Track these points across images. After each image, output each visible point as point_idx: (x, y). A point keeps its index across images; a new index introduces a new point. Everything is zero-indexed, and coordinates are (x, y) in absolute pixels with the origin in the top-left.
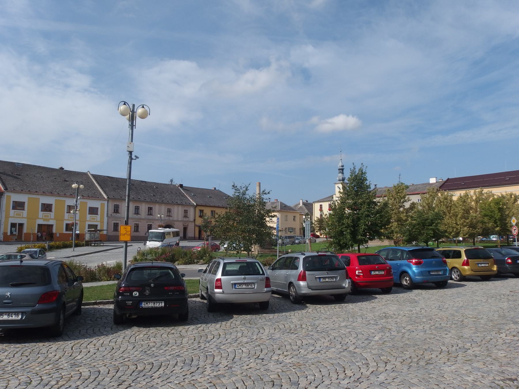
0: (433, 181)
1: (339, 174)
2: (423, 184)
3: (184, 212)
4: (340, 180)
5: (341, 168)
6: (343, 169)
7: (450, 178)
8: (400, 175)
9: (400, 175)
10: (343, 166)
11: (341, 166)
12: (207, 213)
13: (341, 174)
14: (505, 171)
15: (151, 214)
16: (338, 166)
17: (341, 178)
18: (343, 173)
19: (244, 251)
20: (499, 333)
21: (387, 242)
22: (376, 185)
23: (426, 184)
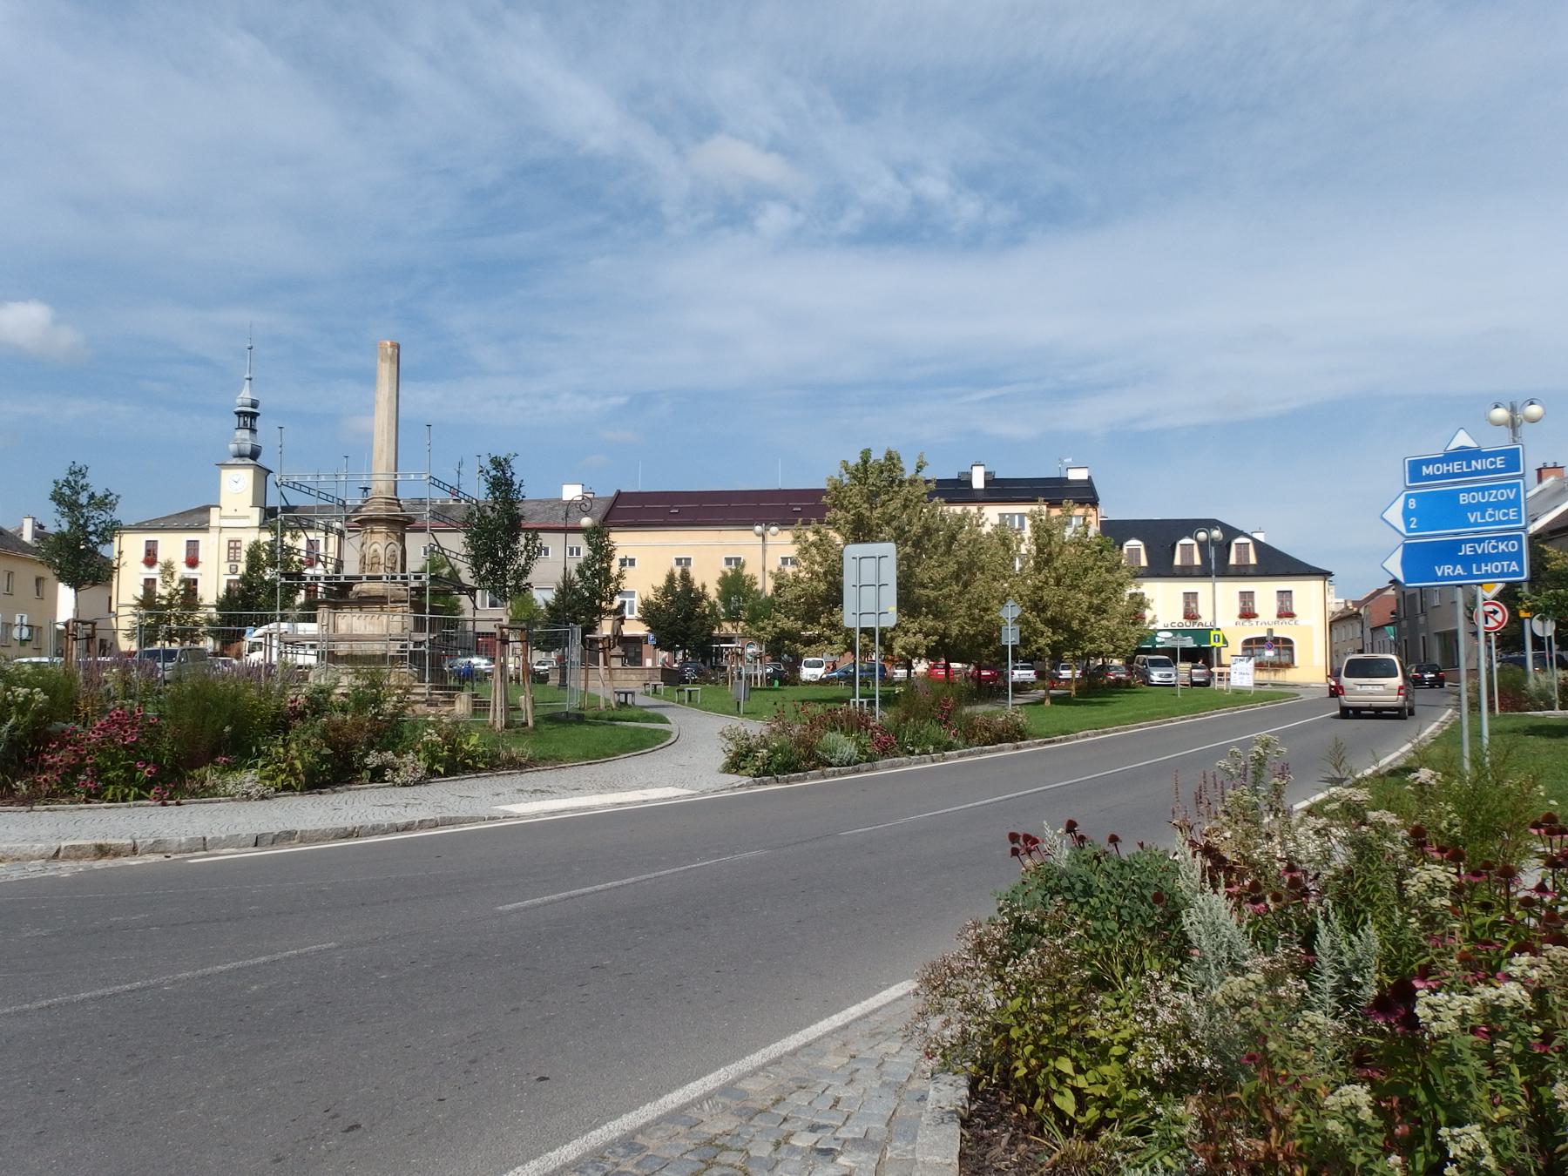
0: (571, 492)
1: (239, 433)
2: (540, 501)
3: (230, 548)
4: (241, 455)
5: (250, 409)
6: (254, 416)
7: (622, 491)
8: (460, 465)
9: (460, 465)
10: (254, 405)
11: (249, 402)
12: (1158, 618)
13: (246, 434)
14: (776, 488)
15: (1243, 594)
16: (239, 401)
17: (248, 448)
18: (253, 431)
19: (1345, 1011)
20: (1522, 980)
21: (634, 677)
22: (366, 489)
23: (548, 501)
